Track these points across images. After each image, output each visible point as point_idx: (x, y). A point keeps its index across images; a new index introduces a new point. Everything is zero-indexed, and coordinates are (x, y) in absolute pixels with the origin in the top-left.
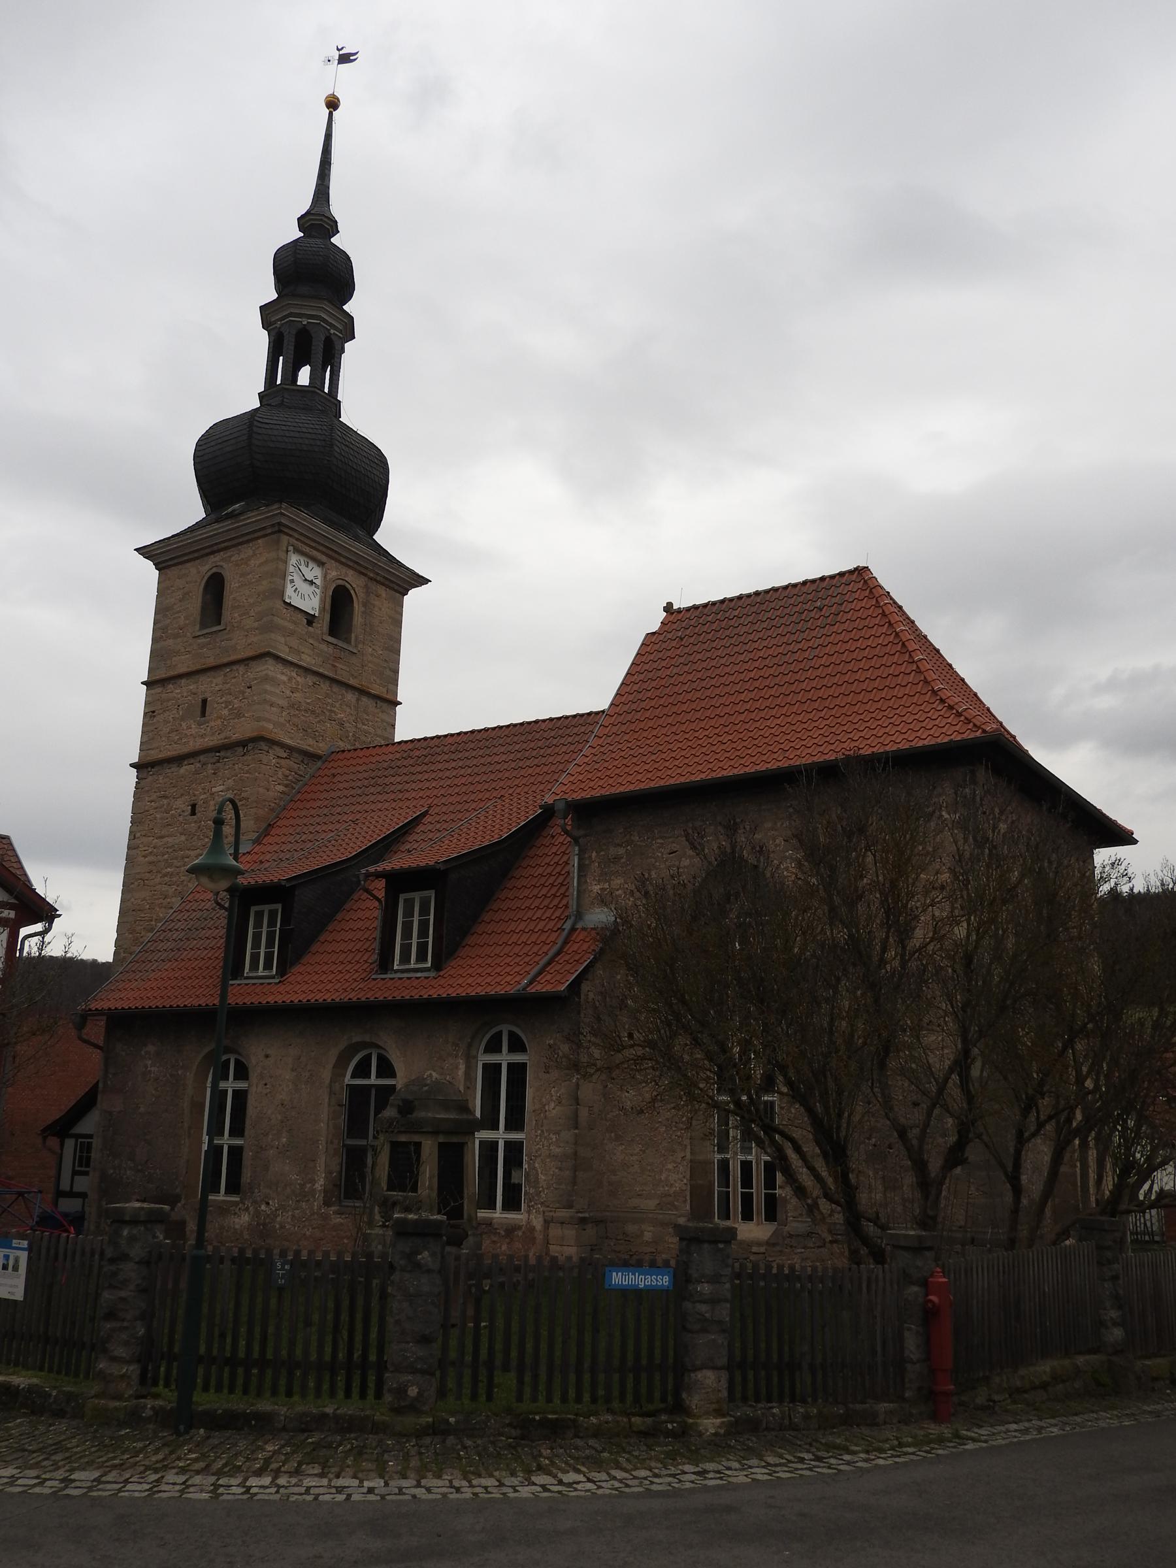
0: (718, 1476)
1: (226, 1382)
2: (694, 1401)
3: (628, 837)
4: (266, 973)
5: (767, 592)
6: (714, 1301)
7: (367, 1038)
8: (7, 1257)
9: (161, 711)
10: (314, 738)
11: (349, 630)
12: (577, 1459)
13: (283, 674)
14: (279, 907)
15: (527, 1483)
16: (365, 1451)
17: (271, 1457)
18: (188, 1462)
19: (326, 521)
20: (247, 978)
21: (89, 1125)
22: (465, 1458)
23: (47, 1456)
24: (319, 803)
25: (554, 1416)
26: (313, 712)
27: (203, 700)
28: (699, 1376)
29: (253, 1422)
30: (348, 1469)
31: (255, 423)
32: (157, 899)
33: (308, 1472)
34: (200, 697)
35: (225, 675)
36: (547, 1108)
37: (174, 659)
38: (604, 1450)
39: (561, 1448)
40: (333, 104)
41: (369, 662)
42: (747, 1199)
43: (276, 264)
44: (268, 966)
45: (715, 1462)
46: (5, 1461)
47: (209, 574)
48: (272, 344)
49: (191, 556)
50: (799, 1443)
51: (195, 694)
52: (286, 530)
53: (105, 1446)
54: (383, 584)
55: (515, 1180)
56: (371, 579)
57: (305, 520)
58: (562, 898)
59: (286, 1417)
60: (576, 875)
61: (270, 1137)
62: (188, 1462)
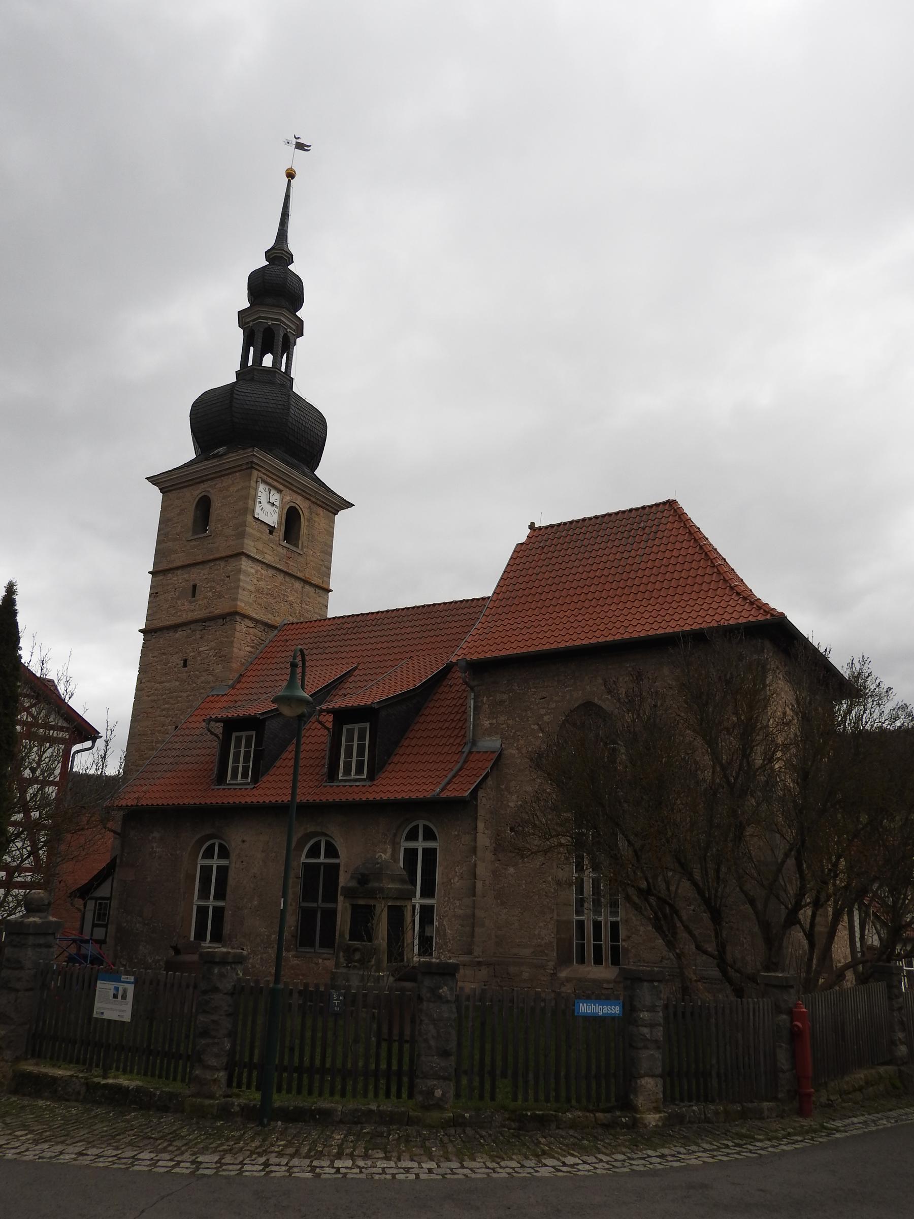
0: (675, 1159)
1: (245, 1080)
2: (640, 1101)
3: (510, 687)
4: (243, 781)
5: (603, 516)
6: (652, 1026)
7: (319, 829)
8: (117, 989)
9: (162, 593)
10: (272, 614)
11: (298, 538)
12: (567, 1145)
13: (252, 567)
14: (254, 733)
15: (541, 1165)
16: (410, 1139)
17: (342, 1144)
18: (281, 1148)
19: (283, 461)
20: (229, 784)
21: (104, 891)
22: (487, 1145)
23: (169, 1143)
24: (275, 660)
25: (541, 1113)
26: (272, 595)
27: (193, 586)
28: (643, 1082)
29: (317, 1116)
30: (404, 1154)
31: (235, 391)
32: (157, 727)
33: (375, 1156)
34: (192, 583)
35: (210, 568)
36: (452, 881)
37: (172, 556)
38: (583, 1138)
39: (551, 1137)
40: (291, 175)
41: (311, 561)
42: (598, 949)
43: (250, 283)
44: (245, 776)
45: (666, 1148)
46: (139, 1147)
47: (200, 496)
48: (246, 338)
49: (186, 484)
50: (717, 1133)
51: (187, 581)
52: (257, 467)
53: (210, 1135)
54: (321, 507)
55: (428, 934)
56: (313, 502)
57: (269, 460)
58: (460, 730)
59: (342, 1112)
60: (472, 714)
61: (245, 900)
62: (281, 1148)
